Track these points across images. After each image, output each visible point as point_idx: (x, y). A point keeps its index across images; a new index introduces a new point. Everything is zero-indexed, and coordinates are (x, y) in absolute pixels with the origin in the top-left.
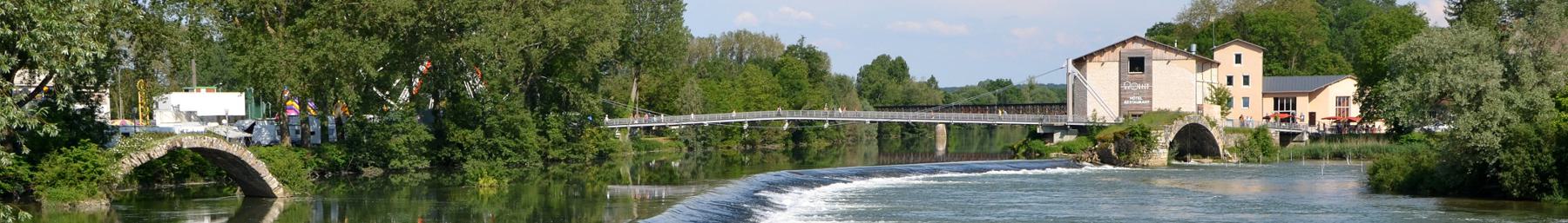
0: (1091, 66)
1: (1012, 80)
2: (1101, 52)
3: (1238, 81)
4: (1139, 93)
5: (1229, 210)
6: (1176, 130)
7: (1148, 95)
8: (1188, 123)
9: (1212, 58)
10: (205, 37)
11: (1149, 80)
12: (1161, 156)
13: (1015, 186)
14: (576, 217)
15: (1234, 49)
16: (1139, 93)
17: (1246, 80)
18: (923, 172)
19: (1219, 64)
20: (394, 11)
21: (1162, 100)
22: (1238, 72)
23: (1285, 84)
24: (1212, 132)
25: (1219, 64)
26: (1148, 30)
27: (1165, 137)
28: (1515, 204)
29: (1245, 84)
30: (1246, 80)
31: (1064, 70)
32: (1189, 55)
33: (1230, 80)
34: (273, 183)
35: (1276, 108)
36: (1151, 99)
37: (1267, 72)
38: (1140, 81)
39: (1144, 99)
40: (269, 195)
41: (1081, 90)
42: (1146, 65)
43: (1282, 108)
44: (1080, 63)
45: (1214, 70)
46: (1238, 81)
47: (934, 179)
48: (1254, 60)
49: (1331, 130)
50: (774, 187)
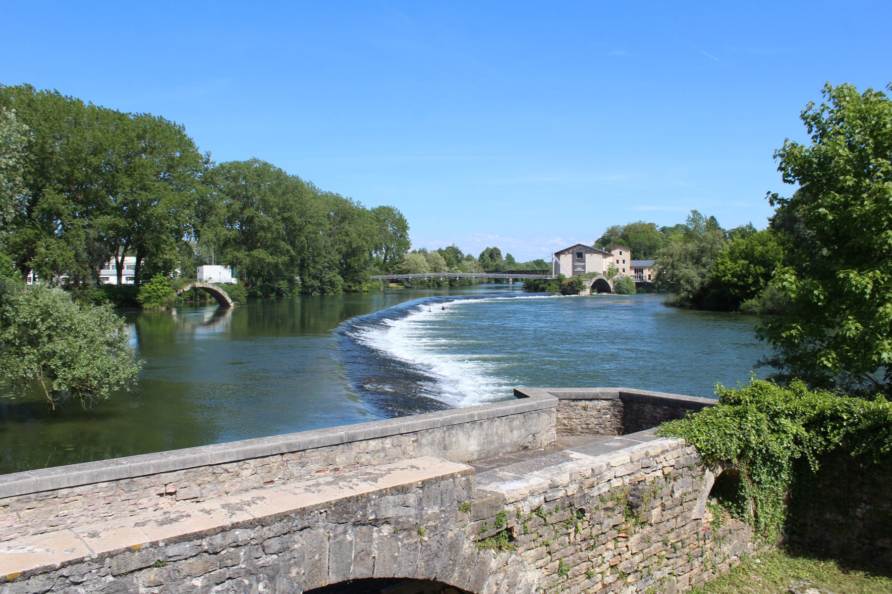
0: (562, 256)
1: (755, 226)
3: (621, 262)
4: (581, 266)
5: (230, 537)
7: (584, 267)
12: (587, 292)
15: (618, 251)
16: (581, 266)
17: (624, 262)
20: (153, 254)
21: (589, 269)
22: (621, 258)
23: (639, 263)
26: (493, 254)
27: (588, 284)
30: (624, 262)
32: (728, 232)
33: (618, 262)
34: (230, 301)
40: (228, 305)
41: (557, 266)
44: (558, 254)
45: (611, 258)
46: (621, 262)
48: (627, 255)
50: (425, 303)
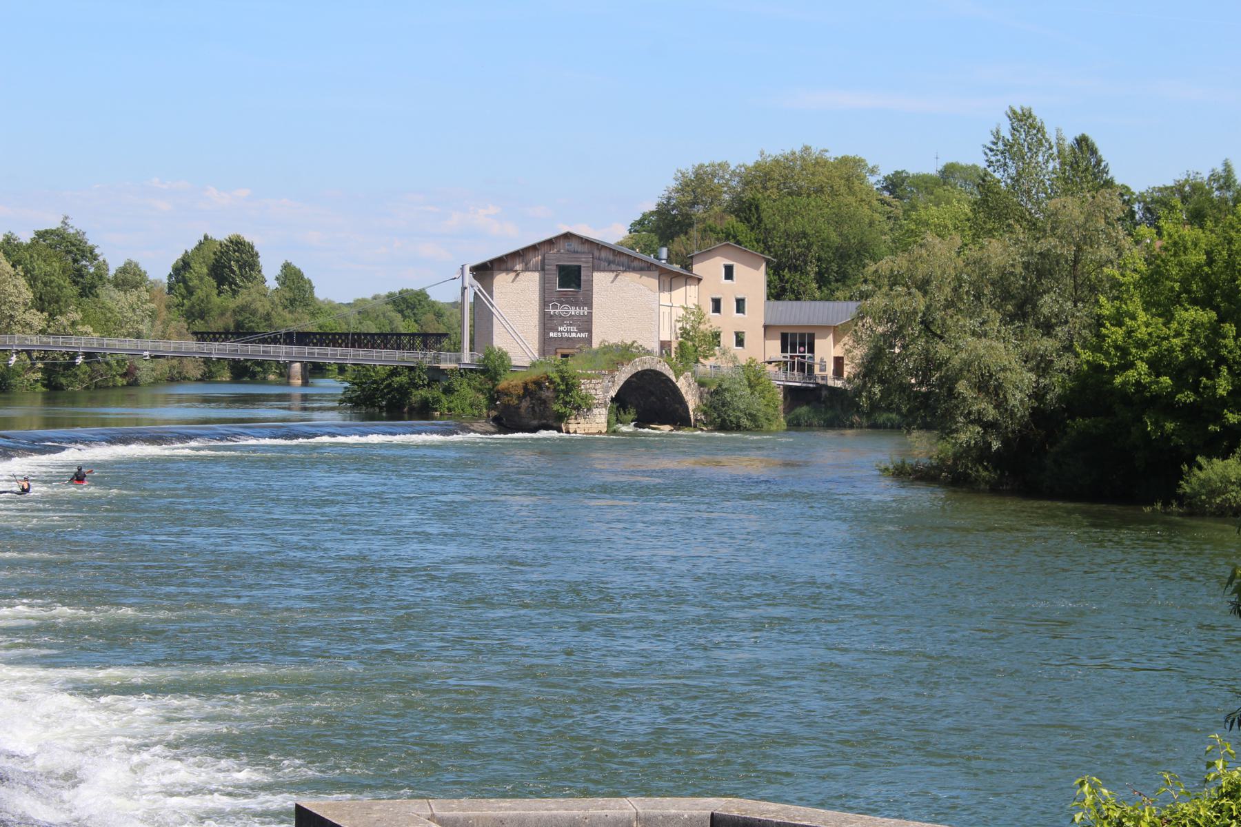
0: (501, 281)
2: (519, 255)
3: (729, 306)
4: (572, 320)
6: (623, 375)
7: (586, 324)
8: (640, 369)
9: (691, 271)
10: (522, 410)
11: (589, 303)
12: (596, 422)
13: (270, 463)
14: (1040, 508)
17: (740, 305)
18: (212, 437)
19: (699, 280)
21: (605, 331)
22: (728, 291)
24: (678, 384)
25: (699, 280)
28: (119, 392)
29: (738, 311)
30: (740, 305)
31: (458, 283)
35: (784, 350)
36: (590, 332)
37: (776, 292)
38: (575, 303)
39: (580, 331)
41: (482, 315)
42: (583, 278)
43: (793, 350)
44: (484, 271)
46: (729, 306)
47: (210, 448)
49: (1013, 432)
